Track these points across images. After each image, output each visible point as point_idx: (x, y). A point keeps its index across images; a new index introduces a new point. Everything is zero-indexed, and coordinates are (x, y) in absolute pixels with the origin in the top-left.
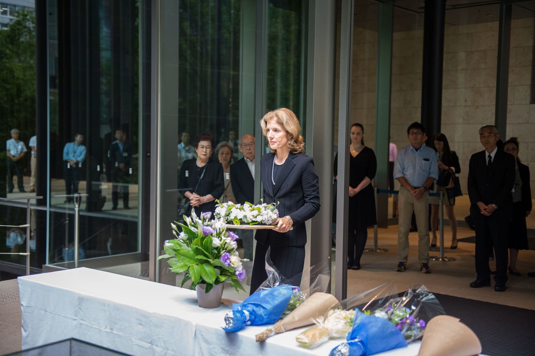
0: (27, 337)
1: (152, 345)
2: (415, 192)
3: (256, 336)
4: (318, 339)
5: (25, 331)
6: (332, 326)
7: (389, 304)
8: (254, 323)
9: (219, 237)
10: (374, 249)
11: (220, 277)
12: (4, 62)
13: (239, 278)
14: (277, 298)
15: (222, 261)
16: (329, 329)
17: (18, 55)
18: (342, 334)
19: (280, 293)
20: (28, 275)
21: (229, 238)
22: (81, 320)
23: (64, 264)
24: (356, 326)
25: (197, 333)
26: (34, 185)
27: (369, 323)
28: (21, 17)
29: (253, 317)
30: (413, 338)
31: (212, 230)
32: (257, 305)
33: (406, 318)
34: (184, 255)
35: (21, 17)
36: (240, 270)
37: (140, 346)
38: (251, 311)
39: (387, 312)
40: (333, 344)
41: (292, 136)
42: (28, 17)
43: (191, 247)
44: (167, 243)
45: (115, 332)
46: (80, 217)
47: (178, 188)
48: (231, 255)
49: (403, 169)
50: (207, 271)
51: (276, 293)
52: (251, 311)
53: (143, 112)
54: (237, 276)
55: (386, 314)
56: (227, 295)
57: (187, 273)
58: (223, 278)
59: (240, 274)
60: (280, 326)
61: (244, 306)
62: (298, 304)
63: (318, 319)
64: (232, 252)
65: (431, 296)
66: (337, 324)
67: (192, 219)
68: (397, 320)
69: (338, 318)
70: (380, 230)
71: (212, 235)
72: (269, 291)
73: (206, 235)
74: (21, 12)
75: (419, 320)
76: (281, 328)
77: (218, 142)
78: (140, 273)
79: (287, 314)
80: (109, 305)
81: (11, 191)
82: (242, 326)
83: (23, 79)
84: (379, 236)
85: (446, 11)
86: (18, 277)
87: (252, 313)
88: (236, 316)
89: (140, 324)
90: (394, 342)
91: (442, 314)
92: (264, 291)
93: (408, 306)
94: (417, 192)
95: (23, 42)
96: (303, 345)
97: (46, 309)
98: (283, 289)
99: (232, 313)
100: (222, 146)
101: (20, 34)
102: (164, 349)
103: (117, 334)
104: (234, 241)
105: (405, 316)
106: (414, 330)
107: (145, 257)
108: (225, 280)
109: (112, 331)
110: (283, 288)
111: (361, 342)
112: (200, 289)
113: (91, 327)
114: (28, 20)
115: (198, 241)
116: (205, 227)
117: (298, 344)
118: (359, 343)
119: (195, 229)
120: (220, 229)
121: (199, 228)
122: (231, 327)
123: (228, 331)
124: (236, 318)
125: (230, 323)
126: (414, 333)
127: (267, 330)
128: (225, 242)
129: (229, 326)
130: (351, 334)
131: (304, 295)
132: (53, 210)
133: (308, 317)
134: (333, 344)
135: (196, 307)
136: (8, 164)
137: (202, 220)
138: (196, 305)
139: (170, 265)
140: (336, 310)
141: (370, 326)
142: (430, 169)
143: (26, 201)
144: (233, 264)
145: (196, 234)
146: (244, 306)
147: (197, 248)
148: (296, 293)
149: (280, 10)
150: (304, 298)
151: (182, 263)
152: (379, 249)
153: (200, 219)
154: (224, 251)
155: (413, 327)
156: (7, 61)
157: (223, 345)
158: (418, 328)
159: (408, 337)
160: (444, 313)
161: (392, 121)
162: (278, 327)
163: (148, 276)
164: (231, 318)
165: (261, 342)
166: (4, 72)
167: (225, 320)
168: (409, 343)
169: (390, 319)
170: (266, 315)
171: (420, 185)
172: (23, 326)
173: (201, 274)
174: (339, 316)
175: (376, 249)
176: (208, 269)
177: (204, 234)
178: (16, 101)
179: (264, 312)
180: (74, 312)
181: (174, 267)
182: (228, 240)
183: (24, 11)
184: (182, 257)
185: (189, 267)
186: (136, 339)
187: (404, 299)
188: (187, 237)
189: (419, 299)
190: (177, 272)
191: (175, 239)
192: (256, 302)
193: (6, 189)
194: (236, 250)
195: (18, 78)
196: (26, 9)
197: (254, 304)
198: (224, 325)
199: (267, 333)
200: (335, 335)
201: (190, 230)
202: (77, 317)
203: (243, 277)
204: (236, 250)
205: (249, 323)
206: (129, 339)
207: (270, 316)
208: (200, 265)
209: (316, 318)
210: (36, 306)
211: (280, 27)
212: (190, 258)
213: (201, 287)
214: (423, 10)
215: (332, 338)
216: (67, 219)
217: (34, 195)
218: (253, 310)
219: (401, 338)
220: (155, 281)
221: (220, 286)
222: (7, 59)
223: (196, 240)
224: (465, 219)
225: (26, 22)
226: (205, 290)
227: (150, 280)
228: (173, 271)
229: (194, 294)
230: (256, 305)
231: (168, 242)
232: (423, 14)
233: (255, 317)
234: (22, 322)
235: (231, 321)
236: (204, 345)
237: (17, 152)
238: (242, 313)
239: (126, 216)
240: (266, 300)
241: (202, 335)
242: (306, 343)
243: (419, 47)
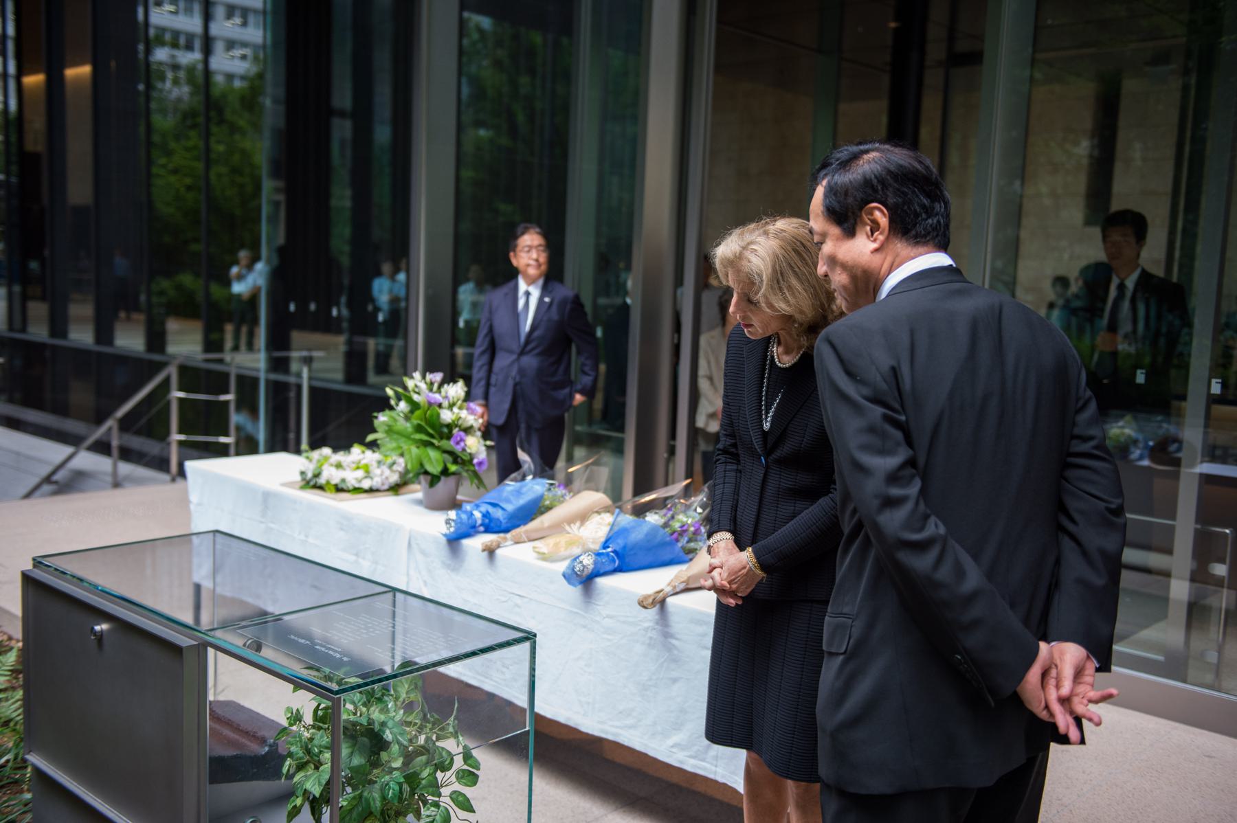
4: (562, 549)
25: (414, 545)
45: (311, 540)
59: (480, 464)
66: (597, 532)
69: (600, 524)
76: (521, 536)
87: (486, 515)
88: (460, 518)
90: (667, 557)
106: (700, 541)
116: (430, 394)
117: (535, 555)
118: (612, 554)
135: (421, 509)
144: (470, 448)
162: (517, 535)
164: (453, 520)
169: (666, 525)
176: (433, 454)
182: (464, 414)
184: (395, 436)
198: (444, 529)
199: (497, 541)
203: (485, 467)
212: (408, 437)
218: (488, 512)
235: (453, 524)
242: (544, 554)
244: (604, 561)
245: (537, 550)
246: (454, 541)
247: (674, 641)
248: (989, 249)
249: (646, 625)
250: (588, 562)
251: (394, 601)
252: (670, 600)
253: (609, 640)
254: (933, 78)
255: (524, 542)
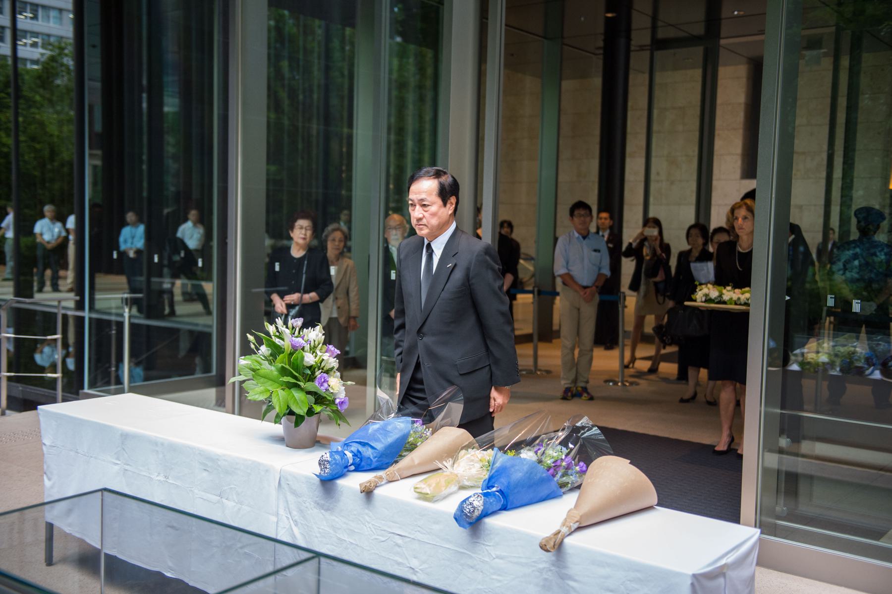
0: (52, 487)
1: (221, 498)
2: (585, 293)
3: (361, 485)
4: (443, 489)
5: (49, 479)
6: (464, 471)
7: (540, 441)
8: (358, 469)
9: (314, 352)
10: (532, 371)
11: (314, 406)
12: (33, 113)
13: (339, 408)
14: (391, 434)
15: (317, 384)
16: (459, 475)
17: (51, 103)
18: (476, 482)
19: (396, 428)
20: (59, 403)
21: (327, 354)
22: (124, 464)
23: (110, 389)
24: (493, 471)
25: (282, 483)
26: (72, 283)
27: (513, 466)
28: (57, 51)
29: (359, 459)
30: (569, 485)
31: (304, 342)
32: (364, 444)
33: (562, 459)
34: (265, 377)
35: (57, 51)
36: (341, 397)
37: (205, 500)
38: (356, 452)
39: (536, 452)
40: (464, 494)
41: (506, 225)
42: (66, 51)
43: (274, 366)
44: (242, 360)
46: (132, 326)
47: (266, 287)
48: (329, 377)
49: (567, 263)
50: (297, 399)
51: (389, 428)
52: (356, 452)
53: (218, 182)
54: (337, 405)
55: (535, 455)
56: (323, 431)
57: (269, 400)
58: (318, 408)
59: (342, 403)
60: (394, 471)
61: (346, 445)
62: (420, 443)
63: (445, 463)
64: (332, 373)
65: (595, 431)
66: (470, 469)
67: (277, 328)
68: (549, 462)
69: (472, 461)
70: (541, 345)
71: (303, 349)
72: (381, 426)
73: (295, 349)
74: (56, 44)
75: (579, 463)
77: (325, 225)
78: (214, 402)
79: (404, 456)
80: (162, 444)
81: (40, 290)
82: (342, 473)
83: (58, 136)
84: (540, 353)
85: (632, 54)
86: (39, 407)
88: (335, 459)
89: (205, 470)
90: (544, 492)
91: (610, 454)
92: (374, 425)
93: (564, 443)
94: (587, 294)
95: (58, 86)
96: (424, 497)
97: (77, 450)
98: (399, 422)
99: (328, 455)
100: (334, 230)
101: (57, 75)
102: (237, 503)
103: (173, 484)
104: (334, 358)
105: (560, 457)
107: (220, 381)
108: (321, 411)
109: (167, 480)
110: (399, 420)
111: (500, 491)
112: (288, 422)
113: (138, 474)
114: (66, 55)
115: (285, 357)
116: (294, 338)
118: (497, 493)
119: (281, 341)
120: (315, 341)
121: (286, 339)
122: (327, 473)
123: (323, 478)
124: (334, 461)
125: (326, 468)
126: (572, 479)
127: (375, 477)
128: (321, 359)
129: (325, 472)
130: (487, 480)
131: (429, 430)
132: (94, 316)
133: (431, 460)
134: (464, 494)
135: (282, 448)
136: (39, 253)
137: (291, 330)
138: (282, 444)
139: (246, 390)
140: (470, 450)
141: (513, 470)
142: (600, 263)
143: (56, 303)
144: (333, 389)
145: (281, 348)
146: (346, 445)
147: (283, 367)
148: (417, 427)
149: (412, 47)
150: (428, 434)
151: (262, 388)
152: (540, 370)
153: (287, 327)
154: (320, 371)
155: (570, 472)
156: (36, 111)
157: (317, 497)
158: (577, 473)
159: (563, 485)
160: (612, 452)
161: (559, 201)
162: (391, 473)
163: (224, 406)
164: (328, 461)
165: (368, 493)
166: (33, 127)
167: (320, 464)
168: (564, 493)
169: (540, 462)
170: (375, 457)
171: (590, 284)
172: (45, 473)
173: (288, 403)
174: (473, 458)
175: (536, 371)
176: (298, 395)
177: (293, 349)
178: (49, 167)
179: (372, 454)
180: (115, 454)
181: (251, 393)
182: (326, 356)
183: (60, 43)
184: (262, 380)
185: (272, 393)
186: (199, 491)
187: (560, 434)
188: (270, 352)
189: (579, 435)
190: (255, 399)
191: (253, 355)
192: (362, 439)
193: (32, 287)
194: (336, 370)
195: (51, 136)
196: (64, 40)
197: (360, 443)
198: (317, 470)
200: (467, 483)
201: (274, 343)
202: (120, 461)
204: (336, 370)
205: (352, 468)
206: (189, 490)
207: (380, 459)
208: (287, 390)
209: (442, 461)
210: (63, 446)
211: (412, 68)
213: (288, 420)
214: (601, 51)
215: (463, 488)
216: (114, 328)
217: (72, 295)
218: (359, 451)
219: (553, 485)
220: (233, 413)
221: (314, 419)
222: (38, 108)
223: (281, 355)
224: (654, 329)
225: (62, 58)
226: (294, 424)
227: (227, 412)
228: (249, 398)
229: (279, 429)
230: (362, 444)
231: (243, 359)
232: (601, 57)
233: (361, 460)
234: (45, 467)
236: (291, 498)
237: (53, 236)
238: (342, 454)
239: (197, 325)
240: (375, 437)
241: (288, 484)
242: (428, 494)
243: (597, 100)
244: (491, 501)
245: (418, 490)
246: (328, 482)
247: (572, 583)
248: (773, 196)
249: (541, 566)
250: (478, 504)
251: (319, 568)
252: (567, 541)
253: (500, 581)
254: (639, 61)
255: (398, 480)
